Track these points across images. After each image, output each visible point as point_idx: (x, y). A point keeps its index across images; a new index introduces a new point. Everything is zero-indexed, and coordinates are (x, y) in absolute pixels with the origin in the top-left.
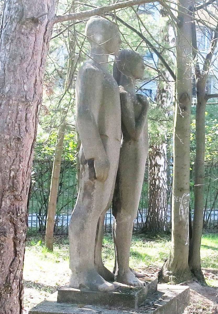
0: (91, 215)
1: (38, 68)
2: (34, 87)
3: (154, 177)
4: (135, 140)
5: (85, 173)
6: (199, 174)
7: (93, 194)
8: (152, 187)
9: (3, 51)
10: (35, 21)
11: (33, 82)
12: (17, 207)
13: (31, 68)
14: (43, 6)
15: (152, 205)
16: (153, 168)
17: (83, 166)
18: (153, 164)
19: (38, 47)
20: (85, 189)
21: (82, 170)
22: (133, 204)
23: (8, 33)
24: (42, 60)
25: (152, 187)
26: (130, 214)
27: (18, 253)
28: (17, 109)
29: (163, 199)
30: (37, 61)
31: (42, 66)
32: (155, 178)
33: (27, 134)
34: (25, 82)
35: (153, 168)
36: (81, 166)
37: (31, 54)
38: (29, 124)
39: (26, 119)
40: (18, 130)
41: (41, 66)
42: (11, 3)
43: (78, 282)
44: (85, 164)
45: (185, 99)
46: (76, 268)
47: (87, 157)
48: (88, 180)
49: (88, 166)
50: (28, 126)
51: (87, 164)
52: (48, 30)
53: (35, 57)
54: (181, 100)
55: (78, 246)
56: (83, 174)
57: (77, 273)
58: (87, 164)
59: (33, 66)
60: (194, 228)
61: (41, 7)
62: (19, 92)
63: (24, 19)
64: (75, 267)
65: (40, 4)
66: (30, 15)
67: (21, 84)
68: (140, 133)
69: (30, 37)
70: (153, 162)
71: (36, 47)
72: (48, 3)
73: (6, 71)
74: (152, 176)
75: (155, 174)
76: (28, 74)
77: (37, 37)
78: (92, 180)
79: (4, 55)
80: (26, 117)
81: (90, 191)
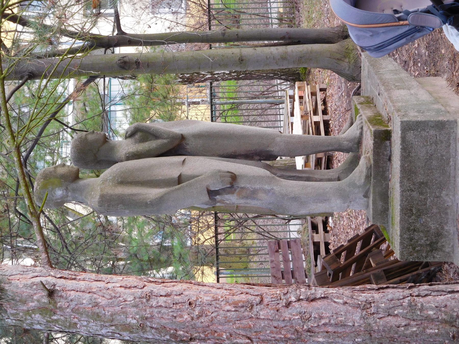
0: (277, 189)
1: (106, 285)
2: (130, 288)
3: (227, 74)
4: (182, 137)
5: (227, 200)
6: (221, 37)
7: (252, 188)
8: (241, 76)
9: (88, 328)
10: (51, 293)
11: (123, 289)
12: (270, 300)
13: (107, 293)
14: (33, 284)
15: (265, 75)
16: (216, 76)
17: (219, 202)
18: (210, 76)
19: (82, 287)
20: (247, 198)
21: (223, 203)
22: (262, 136)
23: (68, 324)
24: (97, 281)
25: (241, 76)
26: (274, 138)
27: (323, 296)
28: (155, 308)
29: (243, 297)
30: (98, 287)
31: (104, 280)
32: (228, 72)
33: (184, 293)
34: (124, 300)
35: (216, 76)
36: (218, 204)
37: (90, 295)
38: (172, 291)
39: (167, 295)
40: (180, 304)
41: (104, 281)
42: (32, 323)
43: (361, 200)
44: (215, 200)
45: (125, 62)
46: (344, 203)
47: (206, 198)
48: (235, 195)
49: (218, 197)
50: (174, 293)
51: (216, 197)
52: (61, 276)
53: (94, 290)
54: (127, 68)
55: (317, 203)
56: (228, 202)
57: (350, 202)
58: (216, 197)
59: (105, 291)
60: (289, 38)
61: (35, 287)
62: (136, 306)
63: (51, 307)
64: (343, 205)
65: (31, 287)
66: (45, 300)
67: (126, 305)
68: (173, 133)
69: (71, 298)
70: (207, 77)
71: (82, 289)
72: (29, 277)
73: (111, 324)
74: (227, 76)
75: (224, 73)
76: (115, 297)
77: (69, 288)
78: (235, 190)
79: (94, 327)
80: (165, 296)
81: (248, 192)
